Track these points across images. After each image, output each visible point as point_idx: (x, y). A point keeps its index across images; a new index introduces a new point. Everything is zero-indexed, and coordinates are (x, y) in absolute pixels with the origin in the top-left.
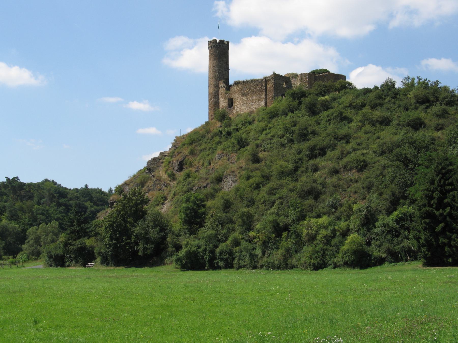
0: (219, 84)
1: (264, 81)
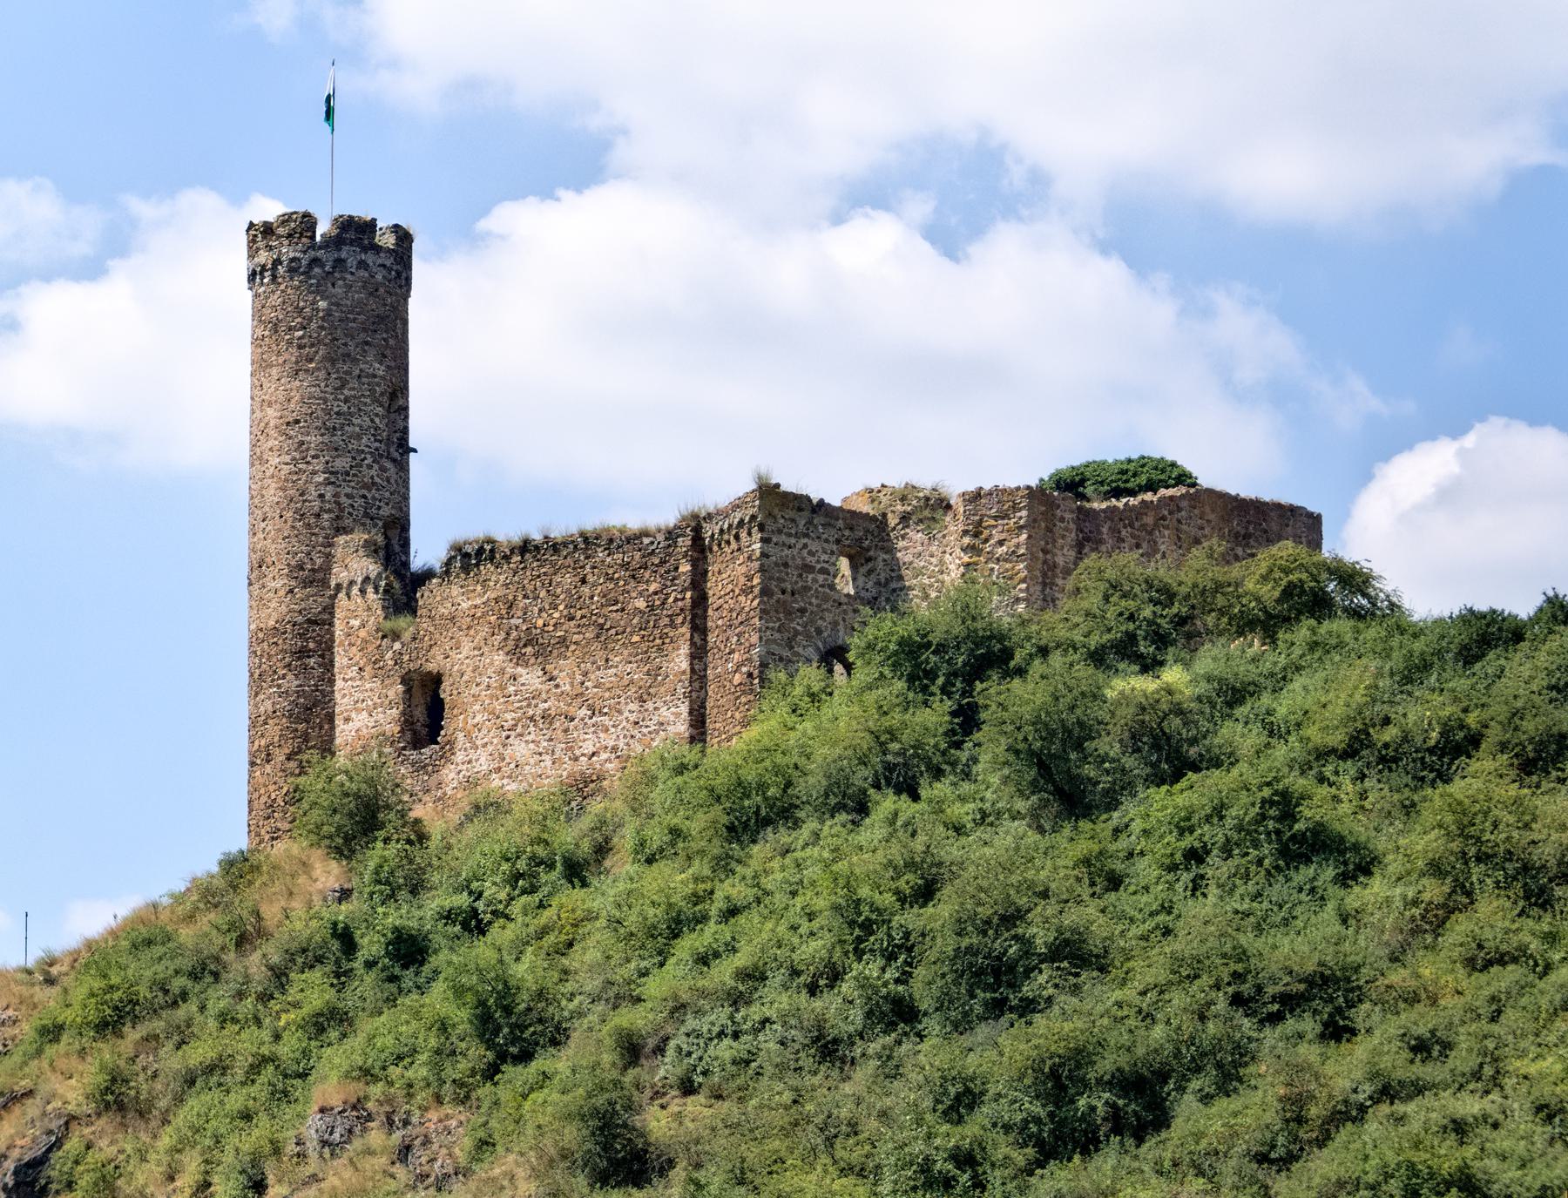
1: (684, 543)
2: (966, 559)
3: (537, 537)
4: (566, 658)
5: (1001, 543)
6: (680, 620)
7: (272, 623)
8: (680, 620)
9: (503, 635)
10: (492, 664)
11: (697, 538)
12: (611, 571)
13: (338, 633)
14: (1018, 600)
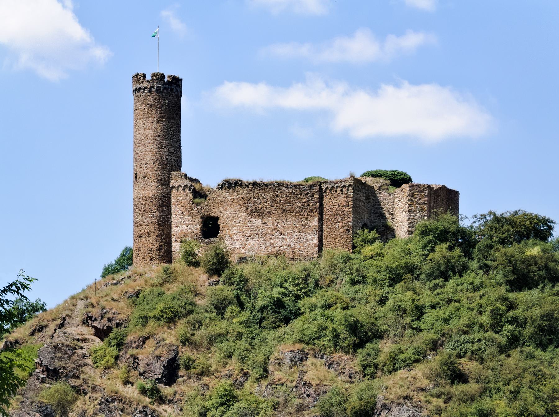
0: (169, 178)
1: (316, 189)
2: (409, 203)
3: (258, 181)
4: (270, 217)
5: (420, 199)
6: (315, 211)
7: (150, 195)
8: (315, 211)
9: (245, 208)
10: (241, 216)
11: (321, 189)
12: (288, 194)
13: (173, 201)
14: (425, 216)
